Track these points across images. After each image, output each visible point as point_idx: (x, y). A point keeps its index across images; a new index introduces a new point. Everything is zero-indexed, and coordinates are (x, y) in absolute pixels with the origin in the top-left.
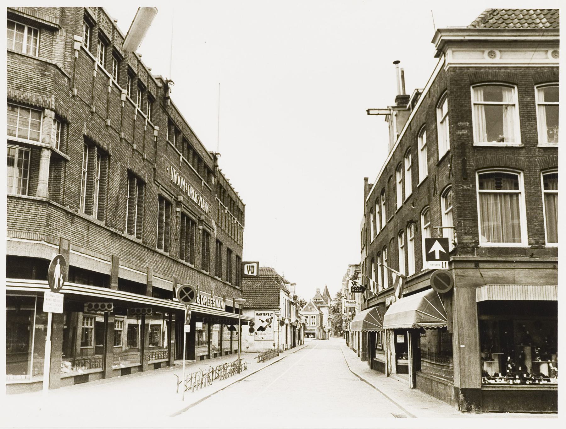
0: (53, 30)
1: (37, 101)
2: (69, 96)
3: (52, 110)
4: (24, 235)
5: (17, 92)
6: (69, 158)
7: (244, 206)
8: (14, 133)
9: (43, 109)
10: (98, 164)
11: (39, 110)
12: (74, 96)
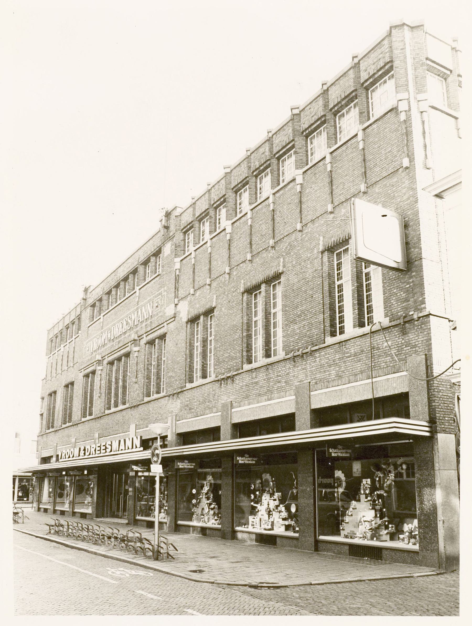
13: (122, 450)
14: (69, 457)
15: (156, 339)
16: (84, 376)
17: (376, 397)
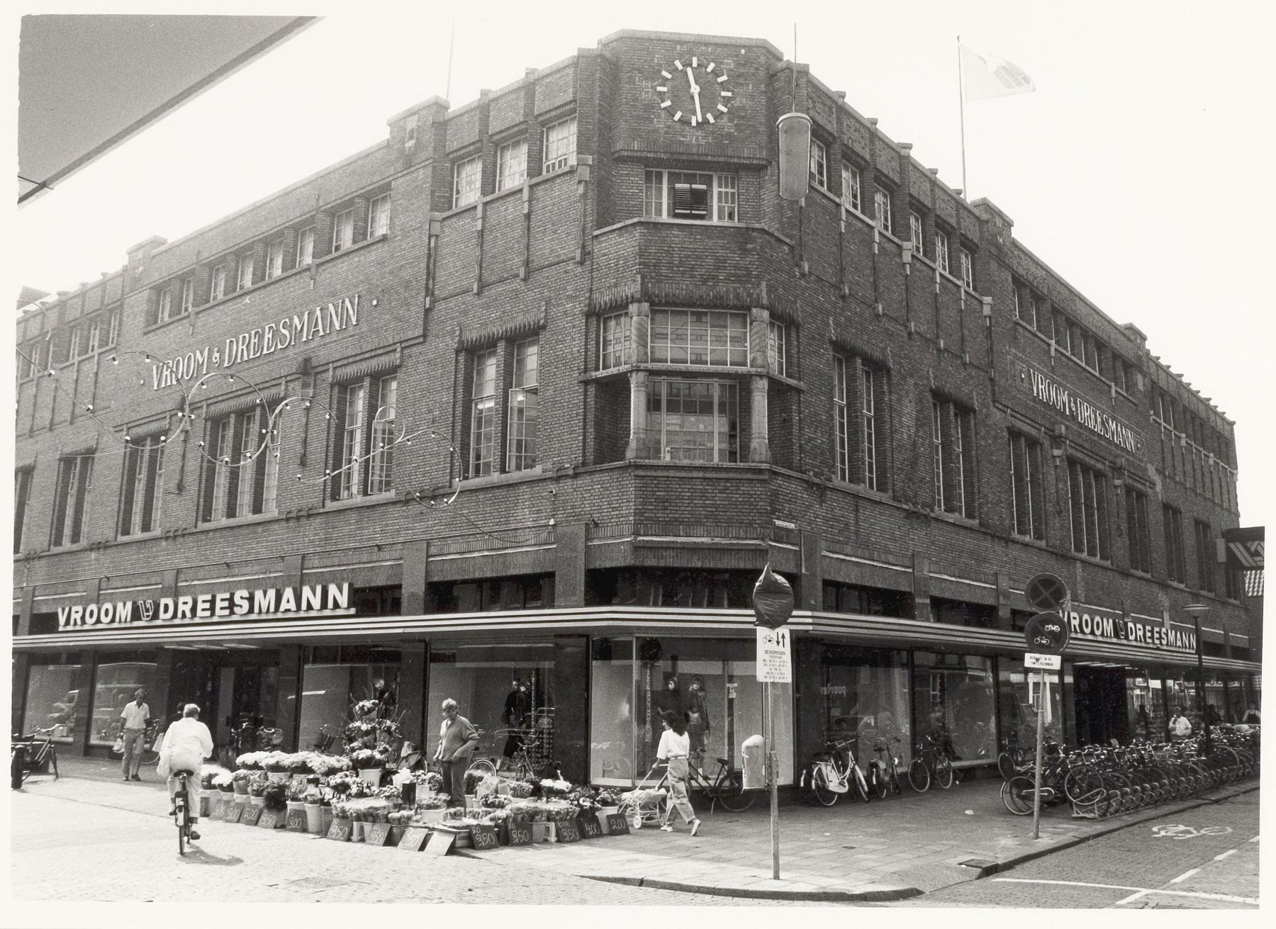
0: (765, 167)
1: (737, 296)
2: (794, 276)
3: (762, 307)
4: (733, 532)
5: (704, 288)
6: (802, 385)
7: (1232, 424)
8: (704, 358)
9: (749, 308)
10: (868, 388)
11: (741, 312)
13: (288, 611)
14: (98, 621)
15: (499, 339)
16: (458, 352)
17: (436, 579)
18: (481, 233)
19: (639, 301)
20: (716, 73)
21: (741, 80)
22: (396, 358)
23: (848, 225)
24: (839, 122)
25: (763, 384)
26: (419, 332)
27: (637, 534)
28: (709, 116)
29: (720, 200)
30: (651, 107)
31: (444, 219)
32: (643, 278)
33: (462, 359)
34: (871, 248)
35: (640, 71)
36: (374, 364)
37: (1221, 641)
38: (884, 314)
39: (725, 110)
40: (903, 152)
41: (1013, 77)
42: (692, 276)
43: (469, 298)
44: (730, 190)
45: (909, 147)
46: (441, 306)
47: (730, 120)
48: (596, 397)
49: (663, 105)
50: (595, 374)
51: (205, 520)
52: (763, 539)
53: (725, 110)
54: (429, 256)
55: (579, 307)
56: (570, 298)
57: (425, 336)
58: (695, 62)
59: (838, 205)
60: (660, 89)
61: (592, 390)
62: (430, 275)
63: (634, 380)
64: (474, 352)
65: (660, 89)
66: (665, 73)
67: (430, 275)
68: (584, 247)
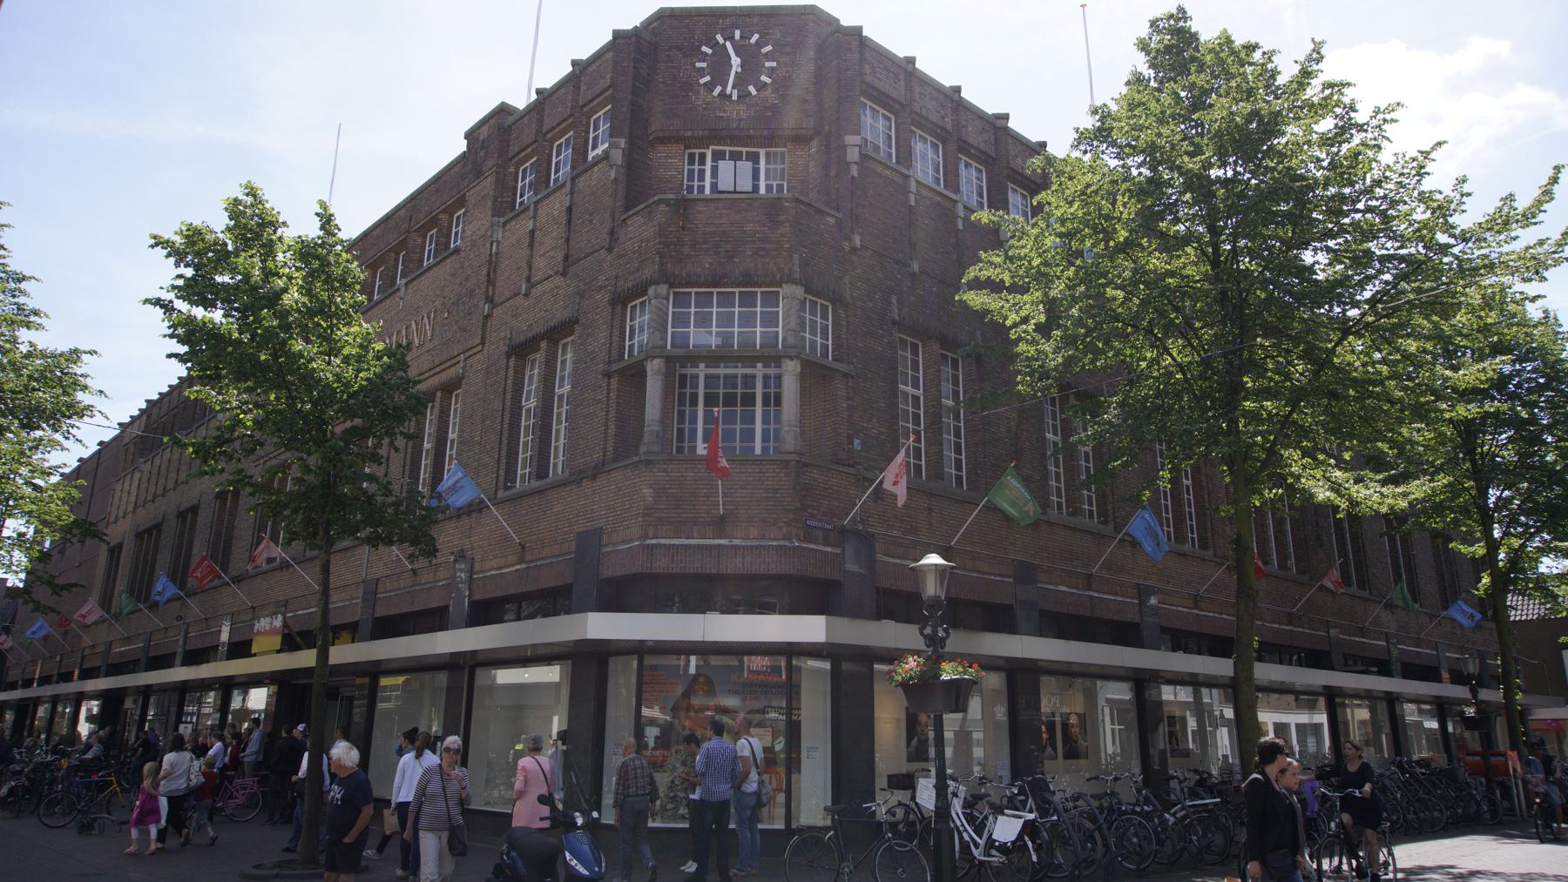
12: (854, 250)
16: (508, 357)
18: (532, 232)
19: (657, 283)
20: (759, 44)
21: (788, 49)
22: (458, 369)
23: (918, 194)
24: (909, 89)
25: (791, 368)
26: (478, 340)
27: (646, 537)
28: (752, 89)
29: (767, 178)
30: (690, 85)
31: (505, 224)
32: (662, 256)
33: (512, 362)
34: (955, 223)
35: (679, 48)
36: (444, 377)
37: (1131, 616)
38: (921, 272)
39: (768, 80)
40: (999, 123)
41: (1083, 6)
42: (716, 253)
43: (519, 300)
44: (779, 166)
45: (1006, 117)
46: (496, 312)
47: (775, 91)
48: (619, 390)
49: (702, 81)
50: (614, 367)
51: (507, 488)
52: (789, 539)
53: (768, 80)
54: (490, 262)
55: (603, 297)
56: (600, 288)
57: (483, 343)
58: (737, 34)
59: (907, 177)
60: (698, 65)
61: (614, 382)
62: (491, 281)
63: (654, 366)
64: (520, 351)
65: (698, 65)
66: (704, 49)
67: (491, 281)
68: (612, 233)
